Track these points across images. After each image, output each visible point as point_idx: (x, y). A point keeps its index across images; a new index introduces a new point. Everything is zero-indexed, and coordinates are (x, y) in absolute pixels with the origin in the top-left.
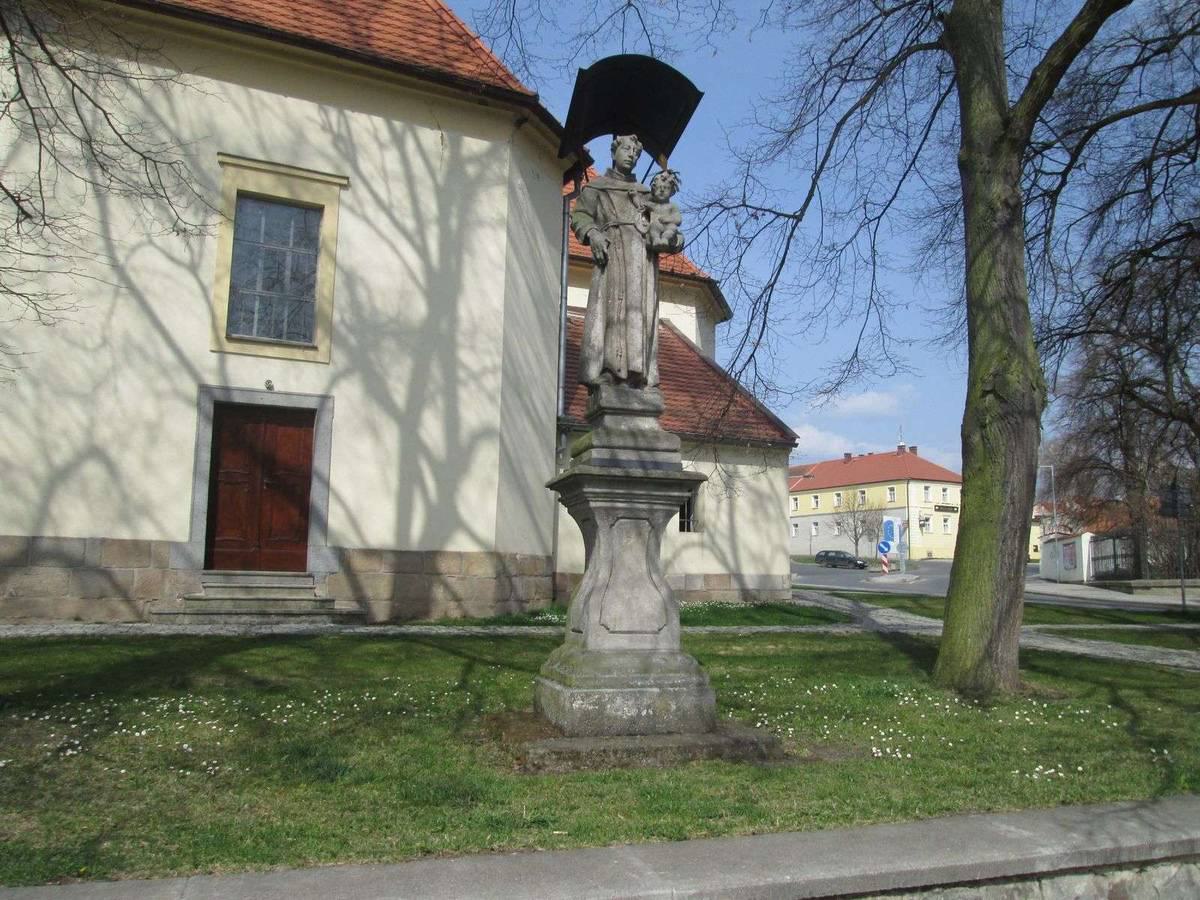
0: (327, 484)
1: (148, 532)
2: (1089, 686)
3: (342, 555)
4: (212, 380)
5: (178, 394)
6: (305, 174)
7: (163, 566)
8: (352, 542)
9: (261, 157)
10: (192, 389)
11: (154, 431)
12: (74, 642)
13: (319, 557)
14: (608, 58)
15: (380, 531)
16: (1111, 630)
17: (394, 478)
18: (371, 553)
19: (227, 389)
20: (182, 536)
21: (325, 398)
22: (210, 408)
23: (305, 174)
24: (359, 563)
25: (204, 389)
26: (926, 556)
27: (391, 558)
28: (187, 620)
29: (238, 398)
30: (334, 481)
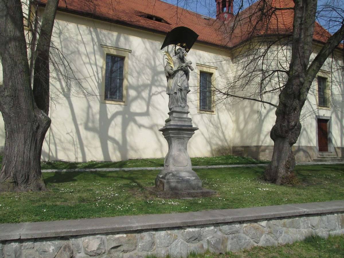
0: (332, 134)
1: (312, 145)
2: (57, 77)
3: (335, 148)
4: (317, 114)
5: (313, 117)
6: (123, 50)
7: (314, 150)
8: (336, 146)
9: (110, 49)
10: (314, 116)
11: (311, 124)
12: (112, 72)
13: (331, 149)
14: (189, 29)
15: (339, 145)
16: (233, 168)
17: (340, 133)
18: (338, 148)
19: (319, 116)
20: (316, 146)
21: (331, 117)
22: (317, 119)
23: (123, 50)
24: (337, 150)
25: (316, 116)
26: (323, 115)
27: (341, 149)
28: (330, 161)
29: (321, 118)
30: (333, 133)
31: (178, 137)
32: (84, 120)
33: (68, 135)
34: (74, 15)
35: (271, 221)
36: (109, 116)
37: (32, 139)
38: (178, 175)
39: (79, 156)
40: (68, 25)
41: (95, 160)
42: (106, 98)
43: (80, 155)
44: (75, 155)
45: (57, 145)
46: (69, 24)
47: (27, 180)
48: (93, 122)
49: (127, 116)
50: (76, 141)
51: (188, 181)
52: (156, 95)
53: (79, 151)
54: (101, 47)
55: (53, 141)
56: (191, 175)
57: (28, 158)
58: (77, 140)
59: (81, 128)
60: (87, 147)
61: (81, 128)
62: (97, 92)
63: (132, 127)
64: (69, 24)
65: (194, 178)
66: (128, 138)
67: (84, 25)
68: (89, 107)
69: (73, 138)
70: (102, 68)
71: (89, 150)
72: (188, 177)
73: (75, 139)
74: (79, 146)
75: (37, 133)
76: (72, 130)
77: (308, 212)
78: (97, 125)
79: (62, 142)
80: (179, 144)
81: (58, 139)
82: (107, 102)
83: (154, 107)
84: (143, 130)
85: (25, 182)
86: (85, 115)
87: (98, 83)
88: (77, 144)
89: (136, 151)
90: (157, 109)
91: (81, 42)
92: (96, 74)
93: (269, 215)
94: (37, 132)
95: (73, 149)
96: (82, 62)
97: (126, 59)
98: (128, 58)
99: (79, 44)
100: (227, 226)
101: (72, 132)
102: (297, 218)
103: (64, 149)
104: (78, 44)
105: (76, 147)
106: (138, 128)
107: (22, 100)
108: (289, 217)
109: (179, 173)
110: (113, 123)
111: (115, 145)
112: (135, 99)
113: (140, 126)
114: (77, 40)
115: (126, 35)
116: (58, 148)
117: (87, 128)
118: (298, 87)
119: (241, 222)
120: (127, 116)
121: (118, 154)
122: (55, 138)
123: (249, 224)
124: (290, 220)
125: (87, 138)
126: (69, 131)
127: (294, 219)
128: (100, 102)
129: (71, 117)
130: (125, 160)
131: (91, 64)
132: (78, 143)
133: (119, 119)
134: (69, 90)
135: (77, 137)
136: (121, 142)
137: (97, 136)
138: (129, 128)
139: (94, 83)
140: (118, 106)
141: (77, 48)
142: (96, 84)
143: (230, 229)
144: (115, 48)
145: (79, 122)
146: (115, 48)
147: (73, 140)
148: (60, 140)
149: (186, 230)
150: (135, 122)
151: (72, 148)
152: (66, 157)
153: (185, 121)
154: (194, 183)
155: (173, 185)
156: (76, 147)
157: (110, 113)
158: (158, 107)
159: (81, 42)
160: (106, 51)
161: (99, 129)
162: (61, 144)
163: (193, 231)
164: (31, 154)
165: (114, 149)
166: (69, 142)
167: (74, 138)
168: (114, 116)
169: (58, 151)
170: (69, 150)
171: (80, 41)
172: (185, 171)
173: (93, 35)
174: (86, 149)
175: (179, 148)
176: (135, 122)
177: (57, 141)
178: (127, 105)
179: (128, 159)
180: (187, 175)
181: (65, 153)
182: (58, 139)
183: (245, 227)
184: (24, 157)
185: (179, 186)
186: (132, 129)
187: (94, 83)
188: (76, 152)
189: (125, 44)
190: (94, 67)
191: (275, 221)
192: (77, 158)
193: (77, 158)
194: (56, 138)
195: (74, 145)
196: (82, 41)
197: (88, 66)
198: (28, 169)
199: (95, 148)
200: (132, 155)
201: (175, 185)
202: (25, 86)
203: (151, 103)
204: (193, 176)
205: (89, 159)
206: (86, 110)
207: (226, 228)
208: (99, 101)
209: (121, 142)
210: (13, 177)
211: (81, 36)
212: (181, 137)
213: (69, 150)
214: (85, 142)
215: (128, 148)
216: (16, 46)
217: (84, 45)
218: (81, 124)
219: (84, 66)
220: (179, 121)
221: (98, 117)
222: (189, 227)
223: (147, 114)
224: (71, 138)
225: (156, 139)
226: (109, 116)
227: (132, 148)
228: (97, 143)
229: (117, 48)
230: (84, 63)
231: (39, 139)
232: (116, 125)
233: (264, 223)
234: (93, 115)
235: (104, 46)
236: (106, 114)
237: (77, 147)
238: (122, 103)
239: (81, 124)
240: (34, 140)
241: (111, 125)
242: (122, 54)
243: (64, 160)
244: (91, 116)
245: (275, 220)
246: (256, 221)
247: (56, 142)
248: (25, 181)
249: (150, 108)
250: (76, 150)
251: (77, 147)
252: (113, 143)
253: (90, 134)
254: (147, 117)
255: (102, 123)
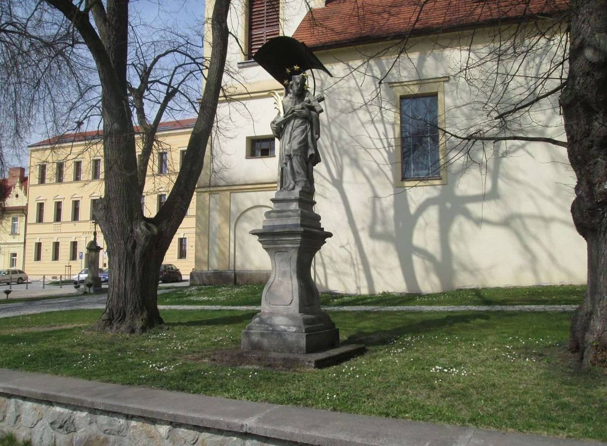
31: (276, 248)
32: (368, 220)
33: (343, 249)
34: (321, 51)
35: (178, 429)
36: (413, 209)
37: (126, 263)
38: (268, 322)
39: (362, 285)
40: (333, 68)
41: (391, 290)
42: (404, 179)
43: (364, 283)
44: (356, 283)
45: (327, 265)
46: (335, 65)
47: (122, 319)
48: (384, 223)
49: (448, 205)
50: (356, 259)
51: (280, 334)
52: (514, 151)
53: (362, 275)
54: (390, 87)
55: (320, 261)
56: (291, 323)
57: (124, 287)
58: (358, 258)
59: (364, 236)
60: (375, 268)
61: (364, 236)
62: (388, 170)
63: (461, 225)
64: (334, 67)
65: (293, 329)
66: (454, 248)
67: (357, 60)
68: (376, 197)
69: (350, 253)
70: (393, 124)
71: (379, 274)
72: (283, 327)
73: (354, 256)
74: (361, 267)
75: (134, 253)
76: (348, 240)
77: (250, 429)
78: (391, 227)
79: (334, 262)
80: (282, 261)
81: (328, 257)
82: (407, 184)
83: (510, 179)
84: (486, 228)
85: (119, 321)
86: (369, 212)
87: (388, 152)
88: (357, 264)
89: (473, 272)
90: (518, 181)
91: (356, 89)
92: (383, 137)
93: (163, 414)
94: (133, 252)
95: (353, 272)
96: (359, 123)
97: (440, 96)
98: (444, 92)
99: (352, 93)
100: (106, 417)
101: (348, 243)
102: (235, 438)
103: (337, 273)
104: (350, 95)
105: (357, 269)
106: (475, 227)
107: (114, 211)
108: (220, 432)
109: (270, 318)
110: (421, 221)
111: (427, 263)
112: (464, 169)
113: (480, 222)
114: (349, 88)
115: (436, 52)
116: (328, 271)
117: (373, 235)
118: (589, 79)
119: (129, 417)
120: (448, 205)
121: (435, 280)
122: (323, 255)
123: (140, 424)
124: (220, 438)
125: (374, 253)
126: (345, 243)
127: (227, 438)
128: (393, 187)
129: (346, 219)
130: (414, 292)
131: (373, 121)
132: (359, 261)
133: (433, 213)
134: (340, 173)
135: (357, 251)
136: (438, 257)
137: (392, 248)
138: (455, 228)
139: (381, 154)
140: (428, 188)
141: (350, 101)
142: (386, 155)
143: (110, 424)
144: (415, 82)
145: (359, 226)
146: (415, 82)
147: (352, 258)
148: (331, 259)
149: (53, 409)
150: (468, 215)
151: (350, 270)
152: (342, 286)
153: (289, 217)
154: (290, 339)
155: (255, 338)
156: (357, 269)
157: (414, 203)
158: (520, 176)
159: (356, 89)
160: (400, 91)
161: (394, 235)
162: (333, 264)
163: (59, 412)
164: (128, 283)
165: (427, 270)
166: (346, 262)
167: (352, 252)
168: (423, 208)
169: (329, 277)
170: (345, 274)
171: (354, 88)
172: (283, 315)
173: (374, 71)
174: (374, 273)
175: (283, 270)
176: (468, 215)
177: (326, 260)
178: (448, 187)
179: (456, 289)
180: (284, 323)
181: (340, 279)
182: (328, 257)
183: (134, 427)
184: (119, 287)
185: (265, 342)
186: (461, 230)
187: (381, 154)
188: (357, 277)
189: (437, 69)
190: (380, 127)
191: (186, 430)
192: (358, 288)
193: (358, 288)
194: (324, 254)
195: (354, 265)
196: (357, 87)
197: (370, 128)
198: (124, 303)
199: (391, 269)
200: (465, 281)
201: (258, 341)
202: (119, 192)
203: (501, 170)
204: (294, 326)
205: (379, 289)
206: (370, 204)
207: (103, 419)
208: (393, 185)
209: (438, 257)
210: (109, 313)
211: (355, 79)
212: (280, 248)
213: (345, 274)
214: (371, 260)
215: (455, 266)
216: (112, 143)
217: (360, 93)
218: (363, 229)
219: (363, 128)
220: (278, 217)
221: (391, 213)
222: (60, 404)
223: (493, 195)
224: (347, 253)
225: (517, 245)
226: (413, 209)
227: (464, 268)
228: (393, 260)
229: (421, 82)
230: (363, 124)
231: (139, 262)
232: (427, 224)
233: (163, 429)
234: (382, 211)
235: (395, 85)
236: (407, 206)
237: (359, 269)
238: (437, 182)
239: (363, 229)
240: (130, 264)
241: (417, 226)
242: (427, 89)
243: (338, 292)
244: (379, 214)
245: (187, 428)
246: (154, 421)
247: (326, 262)
248: (119, 319)
249: (501, 183)
250: (357, 274)
251: (359, 269)
252: (423, 258)
253: (379, 246)
254: (493, 202)
255: (401, 224)
